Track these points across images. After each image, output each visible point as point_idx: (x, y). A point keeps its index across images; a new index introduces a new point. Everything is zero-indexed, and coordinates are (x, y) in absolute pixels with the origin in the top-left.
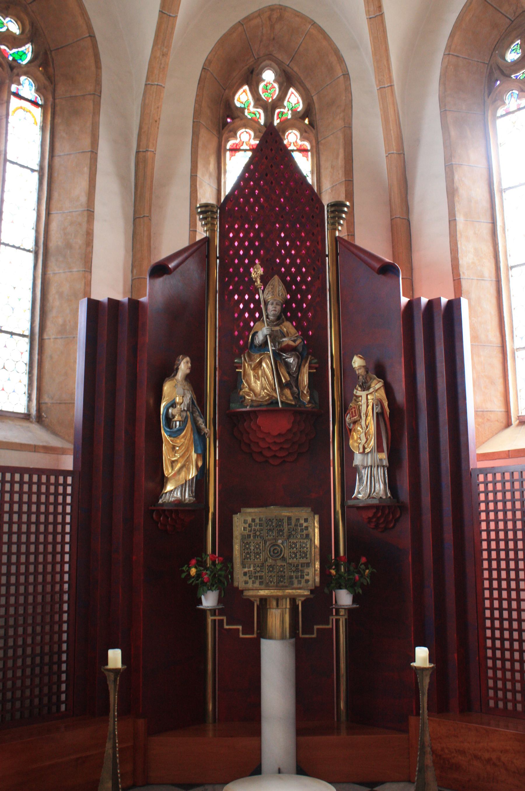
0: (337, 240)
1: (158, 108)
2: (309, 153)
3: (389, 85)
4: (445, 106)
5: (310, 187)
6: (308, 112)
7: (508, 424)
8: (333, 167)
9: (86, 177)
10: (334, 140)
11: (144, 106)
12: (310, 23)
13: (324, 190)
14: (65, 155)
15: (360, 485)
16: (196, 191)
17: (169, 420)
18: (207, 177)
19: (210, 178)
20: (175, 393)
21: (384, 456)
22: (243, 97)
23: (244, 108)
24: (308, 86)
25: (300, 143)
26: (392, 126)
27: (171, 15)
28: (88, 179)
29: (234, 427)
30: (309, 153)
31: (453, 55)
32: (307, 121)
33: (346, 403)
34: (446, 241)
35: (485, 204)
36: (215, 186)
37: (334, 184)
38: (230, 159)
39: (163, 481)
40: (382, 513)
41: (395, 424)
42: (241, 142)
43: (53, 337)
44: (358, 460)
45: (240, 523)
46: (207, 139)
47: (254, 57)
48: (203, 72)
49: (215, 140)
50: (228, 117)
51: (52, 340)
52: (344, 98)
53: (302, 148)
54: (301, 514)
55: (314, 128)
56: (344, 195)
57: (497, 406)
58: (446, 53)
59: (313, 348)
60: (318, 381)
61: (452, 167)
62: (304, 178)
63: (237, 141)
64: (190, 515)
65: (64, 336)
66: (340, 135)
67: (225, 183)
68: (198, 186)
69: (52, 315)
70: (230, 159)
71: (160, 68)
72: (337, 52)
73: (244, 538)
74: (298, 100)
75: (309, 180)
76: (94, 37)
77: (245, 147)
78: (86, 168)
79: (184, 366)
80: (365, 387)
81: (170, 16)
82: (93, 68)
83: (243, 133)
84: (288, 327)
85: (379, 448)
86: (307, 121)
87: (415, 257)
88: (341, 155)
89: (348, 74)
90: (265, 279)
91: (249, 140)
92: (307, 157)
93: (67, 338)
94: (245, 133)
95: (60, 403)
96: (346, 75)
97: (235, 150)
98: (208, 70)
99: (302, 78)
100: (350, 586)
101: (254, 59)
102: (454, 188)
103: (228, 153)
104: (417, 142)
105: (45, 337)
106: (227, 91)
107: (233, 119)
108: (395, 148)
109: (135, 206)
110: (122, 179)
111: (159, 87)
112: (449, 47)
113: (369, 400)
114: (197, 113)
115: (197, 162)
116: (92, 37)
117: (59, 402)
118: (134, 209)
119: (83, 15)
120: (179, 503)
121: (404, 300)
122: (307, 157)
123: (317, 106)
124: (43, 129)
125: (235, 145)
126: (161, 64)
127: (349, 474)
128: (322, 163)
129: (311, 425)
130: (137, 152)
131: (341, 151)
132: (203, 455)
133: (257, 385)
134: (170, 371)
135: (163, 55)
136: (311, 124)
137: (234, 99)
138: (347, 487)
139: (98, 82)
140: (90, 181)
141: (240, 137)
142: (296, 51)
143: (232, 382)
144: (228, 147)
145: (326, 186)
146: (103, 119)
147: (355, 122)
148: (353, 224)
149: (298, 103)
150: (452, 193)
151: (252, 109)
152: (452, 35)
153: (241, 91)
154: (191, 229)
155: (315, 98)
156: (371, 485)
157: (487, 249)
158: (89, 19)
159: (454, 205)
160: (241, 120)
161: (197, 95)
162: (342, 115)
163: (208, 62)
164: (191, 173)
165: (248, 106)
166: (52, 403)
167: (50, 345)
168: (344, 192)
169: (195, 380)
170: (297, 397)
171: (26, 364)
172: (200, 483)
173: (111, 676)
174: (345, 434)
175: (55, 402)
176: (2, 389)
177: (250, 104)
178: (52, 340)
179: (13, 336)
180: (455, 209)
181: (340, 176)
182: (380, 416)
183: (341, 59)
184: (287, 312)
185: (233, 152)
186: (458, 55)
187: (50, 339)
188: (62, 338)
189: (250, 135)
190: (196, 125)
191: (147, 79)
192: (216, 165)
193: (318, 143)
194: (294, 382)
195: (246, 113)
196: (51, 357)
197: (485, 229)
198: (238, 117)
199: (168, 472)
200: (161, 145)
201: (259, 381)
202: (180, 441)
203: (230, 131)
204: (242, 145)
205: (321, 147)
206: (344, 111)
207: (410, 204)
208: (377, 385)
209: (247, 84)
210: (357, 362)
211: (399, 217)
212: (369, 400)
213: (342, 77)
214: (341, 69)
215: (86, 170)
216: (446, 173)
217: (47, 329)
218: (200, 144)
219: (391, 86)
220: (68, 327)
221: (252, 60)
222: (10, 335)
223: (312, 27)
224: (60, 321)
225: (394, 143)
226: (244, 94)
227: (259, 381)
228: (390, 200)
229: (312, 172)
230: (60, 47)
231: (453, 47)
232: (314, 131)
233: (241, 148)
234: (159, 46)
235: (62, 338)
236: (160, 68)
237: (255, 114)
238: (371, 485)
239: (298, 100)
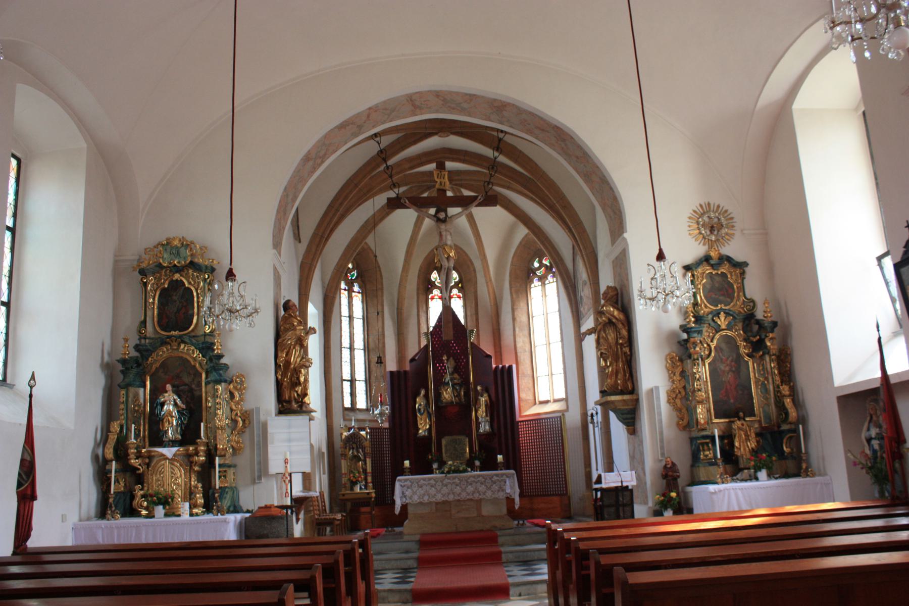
0: (472, 344)
6: (460, 281)
7: (535, 404)
11: (399, 292)
17: (419, 410)
20: (420, 402)
21: (488, 418)
26: (492, 295)
29: (441, 412)
33: (477, 401)
34: (512, 338)
35: (526, 323)
39: (418, 429)
40: (487, 435)
41: (492, 408)
44: (480, 420)
45: (444, 442)
46: (422, 297)
54: (462, 437)
57: (531, 397)
59: (465, 382)
60: (467, 394)
64: (427, 439)
72: (470, 260)
73: (446, 446)
79: (423, 392)
80: (482, 396)
84: (456, 376)
85: (487, 415)
87: (502, 343)
90: (447, 360)
96: (475, 270)
97: (433, 298)
100: (479, 460)
104: (502, 298)
110: (393, 319)
113: (483, 399)
114: (418, 289)
120: (424, 436)
121: (494, 366)
124: (363, 302)
127: (478, 424)
129: (466, 407)
132: (430, 420)
133: (447, 396)
134: (418, 394)
138: (478, 428)
139: (382, 284)
143: (438, 395)
145: (469, 324)
146: (385, 298)
147: (478, 289)
150: (514, 319)
156: (485, 427)
157: (527, 340)
163: (421, 267)
169: (426, 396)
170: (460, 399)
172: (430, 430)
174: (476, 412)
181: (473, 311)
182: (486, 406)
183: (472, 264)
184: (456, 370)
194: (459, 395)
197: (526, 332)
199: (420, 426)
200: (406, 303)
201: (447, 395)
202: (424, 416)
208: (485, 395)
210: (479, 388)
212: (483, 399)
227: (447, 395)
238: (485, 427)
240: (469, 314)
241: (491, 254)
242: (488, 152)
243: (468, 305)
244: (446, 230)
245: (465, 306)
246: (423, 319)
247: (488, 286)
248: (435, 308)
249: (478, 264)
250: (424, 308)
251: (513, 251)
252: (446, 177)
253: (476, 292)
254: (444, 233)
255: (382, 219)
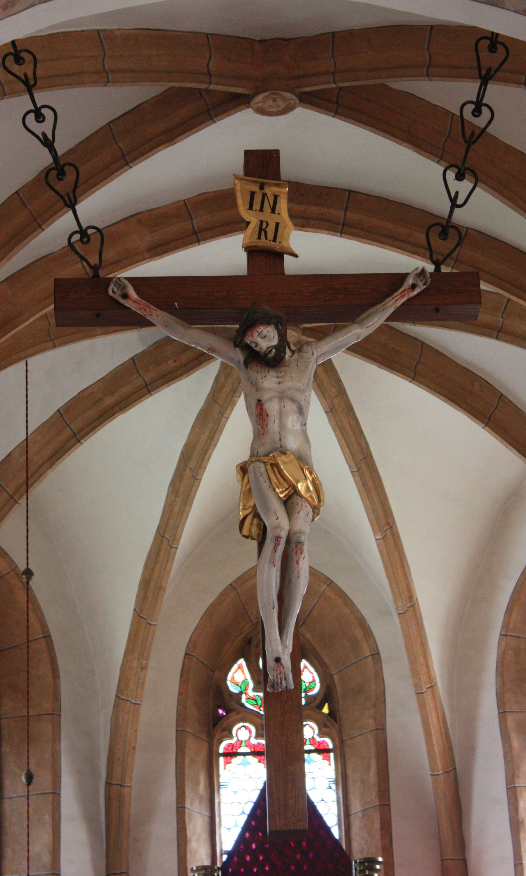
1: (136, 731)
2: (332, 755)
3: (429, 686)
4: (504, 704)
5: (337, 843)
6: (328, 694)
8: (363, 782)
9: (49, 828)
10: (363, 743)
12: (324, 583)
13: (353, 813)
14: (18, 797)
16: (177, 798)
18: (196, 804)
19: (200, 804)
22: (239, 676)
23: (241, 693)
24: (326, 660)
25: (318, 739)
26: (433, 720)
27: (152, 623)
28: (51, 831)
30: (332, 755)
31: (512, 636)
32: (326, 710)
36: (207, 813)
37: (366, 807)
38: (225, 768)
42: (239, 742)
46: (195, 750)
47: (252, 622)
48: (186, 660)
49: (205, 745)
50: (219, 707)
52: (374, 688)
53: (322, 747)
55: (336, 722)
56: (379, 826)
58: (503, 633)
61: (516, 790)
62: (327, 830)
63: (233, 741)
66: (371, 738)
67: (219, 803)
68: (187, 821)
70: (225, 768)
71: (138, 683)
74: (313, 677)
75: (336, 832)
76: (49, 636)
77: (244, 749)
78: (47, 816)
81: (151, 624)
82: (50, 679)
83: (240, 728)
86: (326, 710)
88: (373, 769)
89: (378, 653)
91: (249, 738)
92: (329, 759)
94: (243, 728)
96: (376, 655)
98: (193, 656)
99: (318, 649)
101: (251, 624)
102: (518, 821)
103: (222, 760)
104: (471, 750)
106: (217, 673)
107: (228, 711)
108: (440, 767)
109: (107, 857)
110: (90, 821)
111: (136, 705)
112: (505, 625)
115: (184, 787)
116: (47, 637)
118: (107, 862)
119: (35, 610)
122: (329, 759)
123: (339, 689)
125: (230, 748)
126: (139, 679)
128: (349, 772)
130: (108, 784)
131: (373, 762)
135: (142, 668)
136: (332, 714)
137: (226, 679)
139: (57, 698)
140: (53, 834)
141: (237, 736)
142: (309, 614)
144: (221, 750)
145: (356, 845)
146: (64, 745)
148: (392, 865)
149: (314, 681)
151: (251, 693)
152: (509, 611)
153: (235, 666)
155: (336, 678)
158: (42, 614)
159: (520, 844)
160: (238, 713)
161: (180, 693)
162: (372, 711)
163: (192, 644)
164: (177, 803)
165: (246, 690)
168: (379, 821)
177: (248, 685)
180: (520, 849)
183: (368, 633)
185: (228, 758)
186: (518, 635)
189: (250, 731)
190: (180, 734)
191: (119, 689)
192: (208, 780)
193: (342, 742)
195: (244, 700)
198: (233, 710)
200: (139, 763)
203: (224, 730)
204: (240, 747)
205: (347, 749)
206: (375, 706)
207: (465, 836)
209: (243, 657)
211: (451, 859)
213: (370, 657)
214: (369, 646)
215: (48, 818)
216: (509, 799)
218: (187, 760)
219: (431, 687)
221: (248, 626)
223: (328, 588)
225: (439, 762)
226: (240, 671)
228: (439, 832)
229: (339, 824)
230: (4, 648)
231: (511, 626)
232: (336, 726)
233: (239, 751)
234: (136, 655)
236: (138, 683)
237: (256, 700)
239: (313, 677)
240: (356, 807)
241: (434, 597)
242: (410, 174)
243: (353, 776)
244: (282, 396)
245: (343, 780)
246: (197, 826)
247: (422, 705)
248: (242, 783)
249: (387, 634)
250: (202, 787)
251: (503, 600)
252: (283, 205)
253: (381, 730)
254: (272, 407)
255: (78, 437)
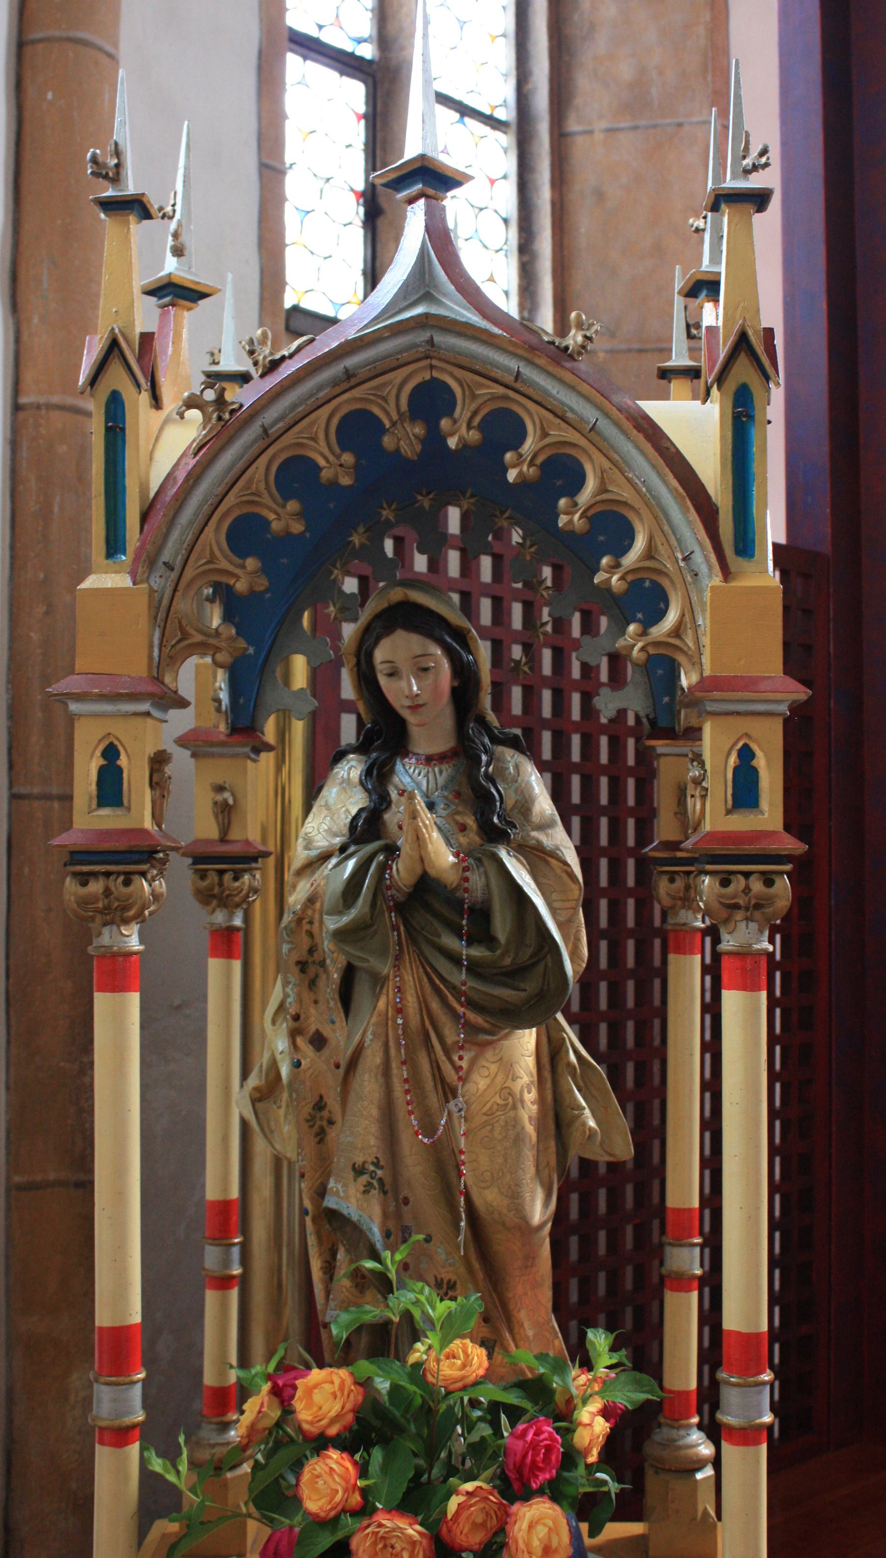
15: (300, 1355)
43: (604, 124)
51: (599, 136)
65: (643, 122)
69: (593, 53)
93: (655, 126)
95: (641, 351)
105: (573, 125)
117: (636, 346)
154: (17, 1179)
166: (612, 352)
167: (591, 155)
171: (506, 221)
173: (383, 1500)
175: (623, 346)
176: (488, 183)
178: (599, 136)
179: (467, 120)
187: (590, 132)
188: (635, 128)
196: (600, 195)
217: (579, 101)
220: (654, 91)
222: (457, 116)
224: (626, 71)
235: (635, 128)
